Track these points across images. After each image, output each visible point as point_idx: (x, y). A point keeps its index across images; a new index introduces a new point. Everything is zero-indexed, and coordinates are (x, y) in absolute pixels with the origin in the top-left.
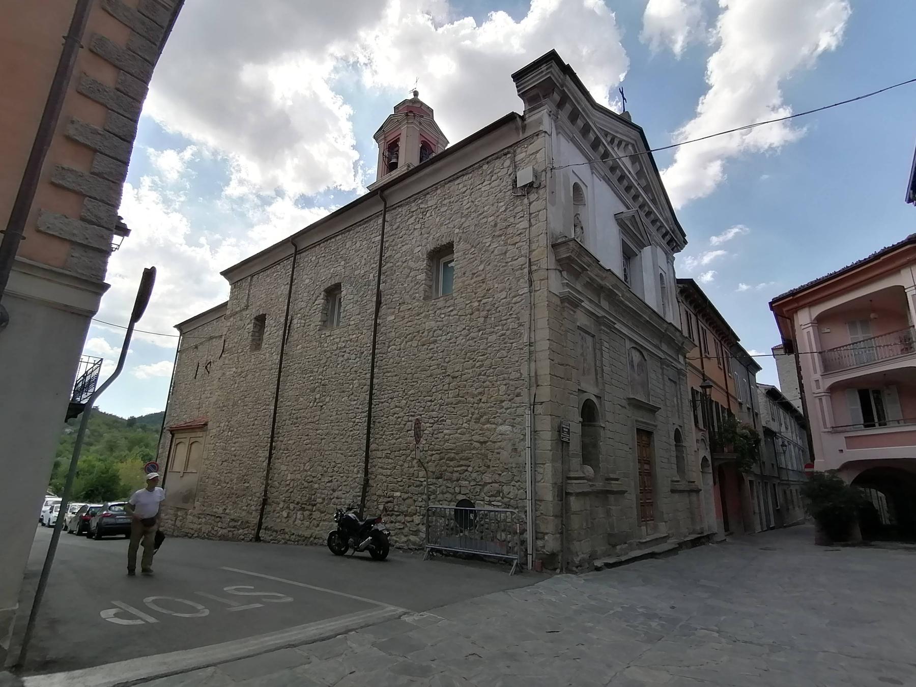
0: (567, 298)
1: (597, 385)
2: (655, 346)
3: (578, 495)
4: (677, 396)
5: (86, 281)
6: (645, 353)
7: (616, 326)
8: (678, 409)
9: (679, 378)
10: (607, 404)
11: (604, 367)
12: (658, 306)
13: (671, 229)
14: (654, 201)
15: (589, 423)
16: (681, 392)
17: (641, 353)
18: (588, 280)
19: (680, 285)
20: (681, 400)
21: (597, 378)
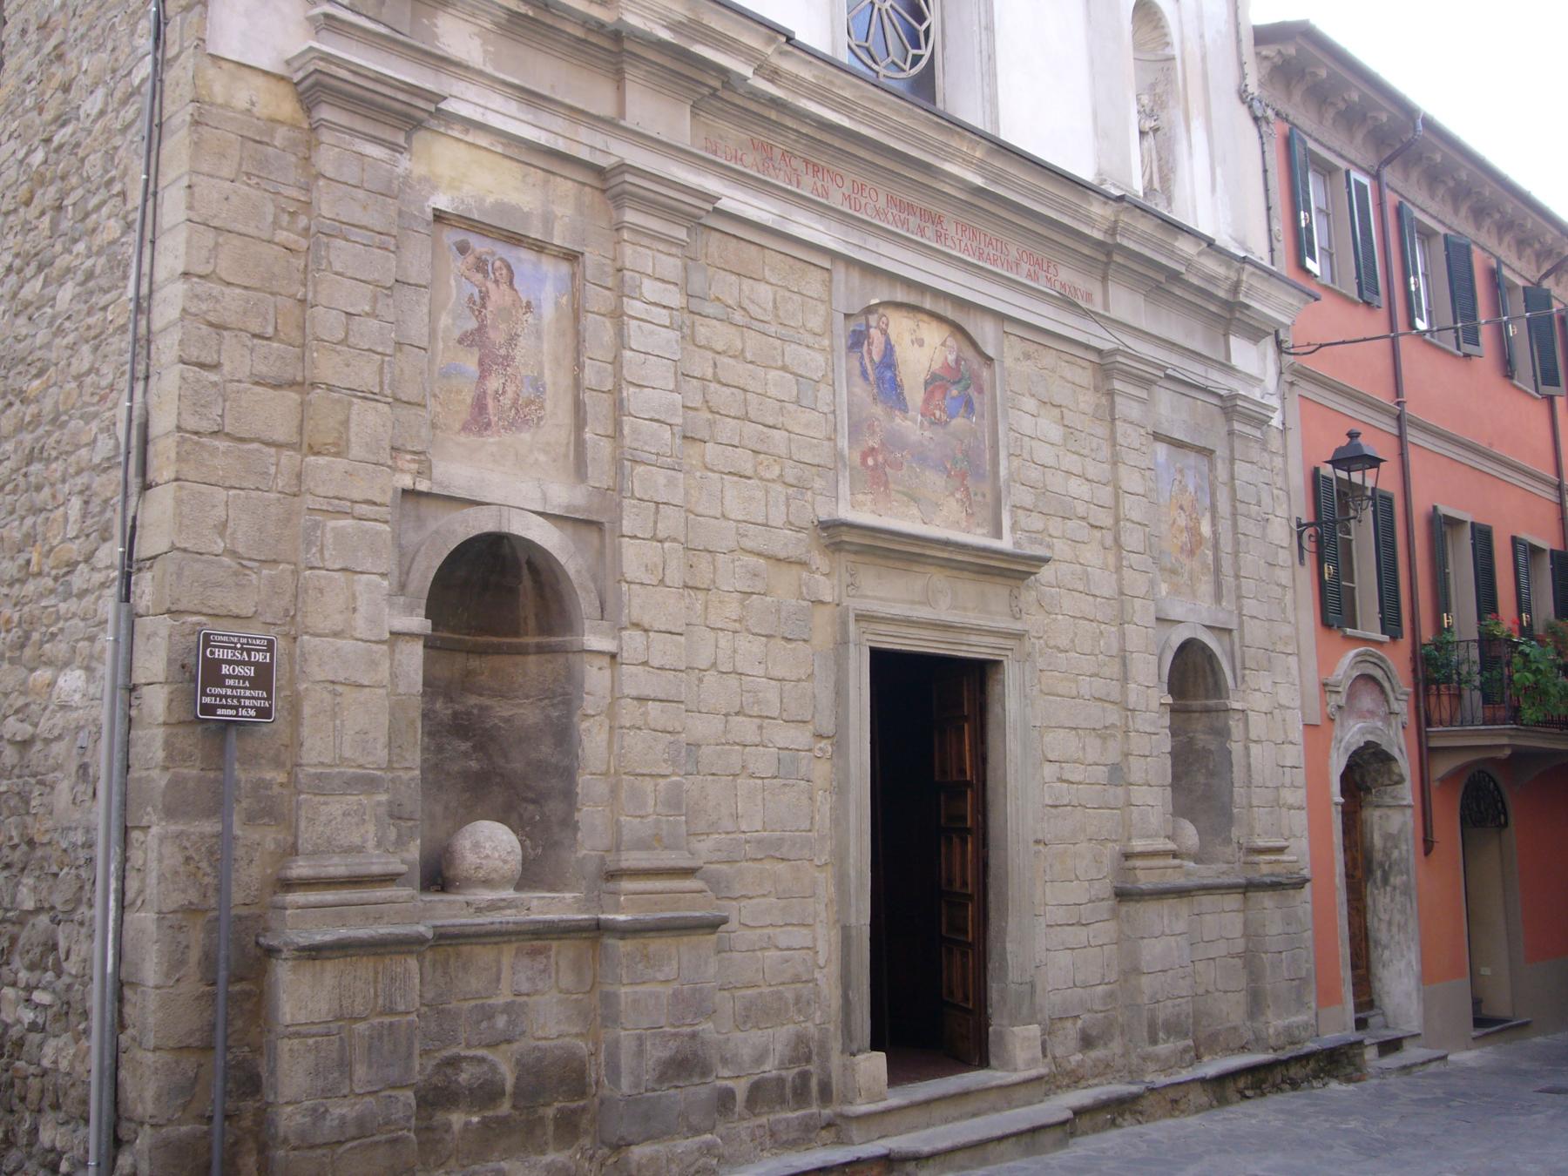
0: (317, 84)
1: (580, 467)
2: (1068, 303)
3: (315, 953)
4: (1213, 508)
5: (116, 1103)
6: (971, 324)
7: (724, 204)
8: (1217, 560)
9: (1231, 433)
10: (634, 558)
11: (629, 392)
12: (1101, 132)
15: (544, 640)
16: (1233, 490)
17: (958, 329)
19: (1265, 52)
20: (1235, 525)
21: (580, 444)
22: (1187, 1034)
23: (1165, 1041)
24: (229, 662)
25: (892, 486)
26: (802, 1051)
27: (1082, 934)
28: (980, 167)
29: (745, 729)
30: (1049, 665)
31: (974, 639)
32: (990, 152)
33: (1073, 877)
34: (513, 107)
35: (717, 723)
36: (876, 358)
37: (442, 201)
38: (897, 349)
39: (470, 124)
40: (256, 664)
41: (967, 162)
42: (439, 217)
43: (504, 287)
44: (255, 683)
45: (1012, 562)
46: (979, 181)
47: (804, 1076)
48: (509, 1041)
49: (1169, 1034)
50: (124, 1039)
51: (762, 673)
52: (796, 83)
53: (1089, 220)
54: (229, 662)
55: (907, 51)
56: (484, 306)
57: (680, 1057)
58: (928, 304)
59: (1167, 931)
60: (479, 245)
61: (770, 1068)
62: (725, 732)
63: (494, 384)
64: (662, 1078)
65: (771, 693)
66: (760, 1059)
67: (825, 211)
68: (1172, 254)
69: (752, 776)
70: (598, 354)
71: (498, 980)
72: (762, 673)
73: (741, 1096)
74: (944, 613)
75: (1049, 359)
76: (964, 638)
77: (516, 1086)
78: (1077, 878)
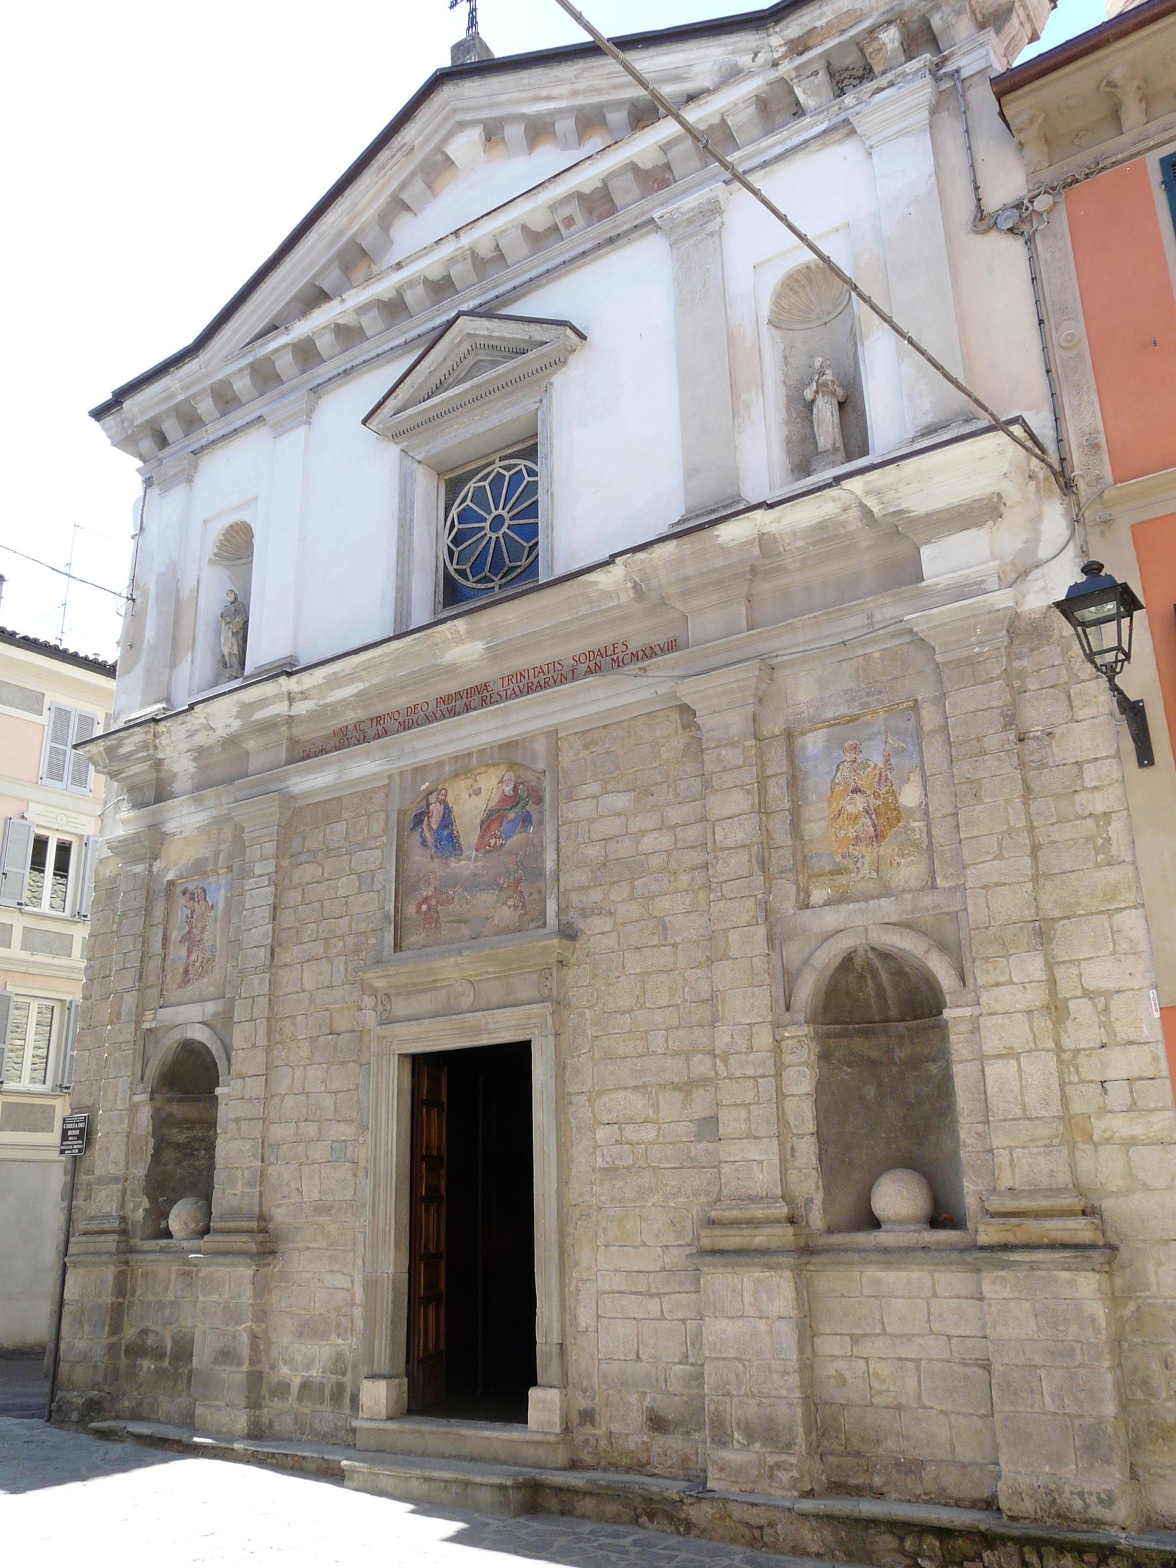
22: (789, 1446)
23: (745, 1448)
24: (71, 1129)
25: (442, 920)
26: (339, 1365)
35: (292, 1127)
36: (434, 826)
38: (455, 809)
40: (80, 1129)
43: (202, 902)
44: (80, 1137)
47: (340, 1386)
48: (171, 1324)
49: (751, 1438)
51: (322, 1089)
54: (71, 1129)
55: (530, 548)
56: (192, 918)
57: (225, 1350)
59: (749, 1311)
61: (315, 1373)
63: (194, 957)
64: (216, 1361)
65: (328, 1102)
66: (308, 1366)
70: (732, 756)
71: (168, 1288)
72: (322, 1089)
73: (295, 1389)
77: (172, 1348)
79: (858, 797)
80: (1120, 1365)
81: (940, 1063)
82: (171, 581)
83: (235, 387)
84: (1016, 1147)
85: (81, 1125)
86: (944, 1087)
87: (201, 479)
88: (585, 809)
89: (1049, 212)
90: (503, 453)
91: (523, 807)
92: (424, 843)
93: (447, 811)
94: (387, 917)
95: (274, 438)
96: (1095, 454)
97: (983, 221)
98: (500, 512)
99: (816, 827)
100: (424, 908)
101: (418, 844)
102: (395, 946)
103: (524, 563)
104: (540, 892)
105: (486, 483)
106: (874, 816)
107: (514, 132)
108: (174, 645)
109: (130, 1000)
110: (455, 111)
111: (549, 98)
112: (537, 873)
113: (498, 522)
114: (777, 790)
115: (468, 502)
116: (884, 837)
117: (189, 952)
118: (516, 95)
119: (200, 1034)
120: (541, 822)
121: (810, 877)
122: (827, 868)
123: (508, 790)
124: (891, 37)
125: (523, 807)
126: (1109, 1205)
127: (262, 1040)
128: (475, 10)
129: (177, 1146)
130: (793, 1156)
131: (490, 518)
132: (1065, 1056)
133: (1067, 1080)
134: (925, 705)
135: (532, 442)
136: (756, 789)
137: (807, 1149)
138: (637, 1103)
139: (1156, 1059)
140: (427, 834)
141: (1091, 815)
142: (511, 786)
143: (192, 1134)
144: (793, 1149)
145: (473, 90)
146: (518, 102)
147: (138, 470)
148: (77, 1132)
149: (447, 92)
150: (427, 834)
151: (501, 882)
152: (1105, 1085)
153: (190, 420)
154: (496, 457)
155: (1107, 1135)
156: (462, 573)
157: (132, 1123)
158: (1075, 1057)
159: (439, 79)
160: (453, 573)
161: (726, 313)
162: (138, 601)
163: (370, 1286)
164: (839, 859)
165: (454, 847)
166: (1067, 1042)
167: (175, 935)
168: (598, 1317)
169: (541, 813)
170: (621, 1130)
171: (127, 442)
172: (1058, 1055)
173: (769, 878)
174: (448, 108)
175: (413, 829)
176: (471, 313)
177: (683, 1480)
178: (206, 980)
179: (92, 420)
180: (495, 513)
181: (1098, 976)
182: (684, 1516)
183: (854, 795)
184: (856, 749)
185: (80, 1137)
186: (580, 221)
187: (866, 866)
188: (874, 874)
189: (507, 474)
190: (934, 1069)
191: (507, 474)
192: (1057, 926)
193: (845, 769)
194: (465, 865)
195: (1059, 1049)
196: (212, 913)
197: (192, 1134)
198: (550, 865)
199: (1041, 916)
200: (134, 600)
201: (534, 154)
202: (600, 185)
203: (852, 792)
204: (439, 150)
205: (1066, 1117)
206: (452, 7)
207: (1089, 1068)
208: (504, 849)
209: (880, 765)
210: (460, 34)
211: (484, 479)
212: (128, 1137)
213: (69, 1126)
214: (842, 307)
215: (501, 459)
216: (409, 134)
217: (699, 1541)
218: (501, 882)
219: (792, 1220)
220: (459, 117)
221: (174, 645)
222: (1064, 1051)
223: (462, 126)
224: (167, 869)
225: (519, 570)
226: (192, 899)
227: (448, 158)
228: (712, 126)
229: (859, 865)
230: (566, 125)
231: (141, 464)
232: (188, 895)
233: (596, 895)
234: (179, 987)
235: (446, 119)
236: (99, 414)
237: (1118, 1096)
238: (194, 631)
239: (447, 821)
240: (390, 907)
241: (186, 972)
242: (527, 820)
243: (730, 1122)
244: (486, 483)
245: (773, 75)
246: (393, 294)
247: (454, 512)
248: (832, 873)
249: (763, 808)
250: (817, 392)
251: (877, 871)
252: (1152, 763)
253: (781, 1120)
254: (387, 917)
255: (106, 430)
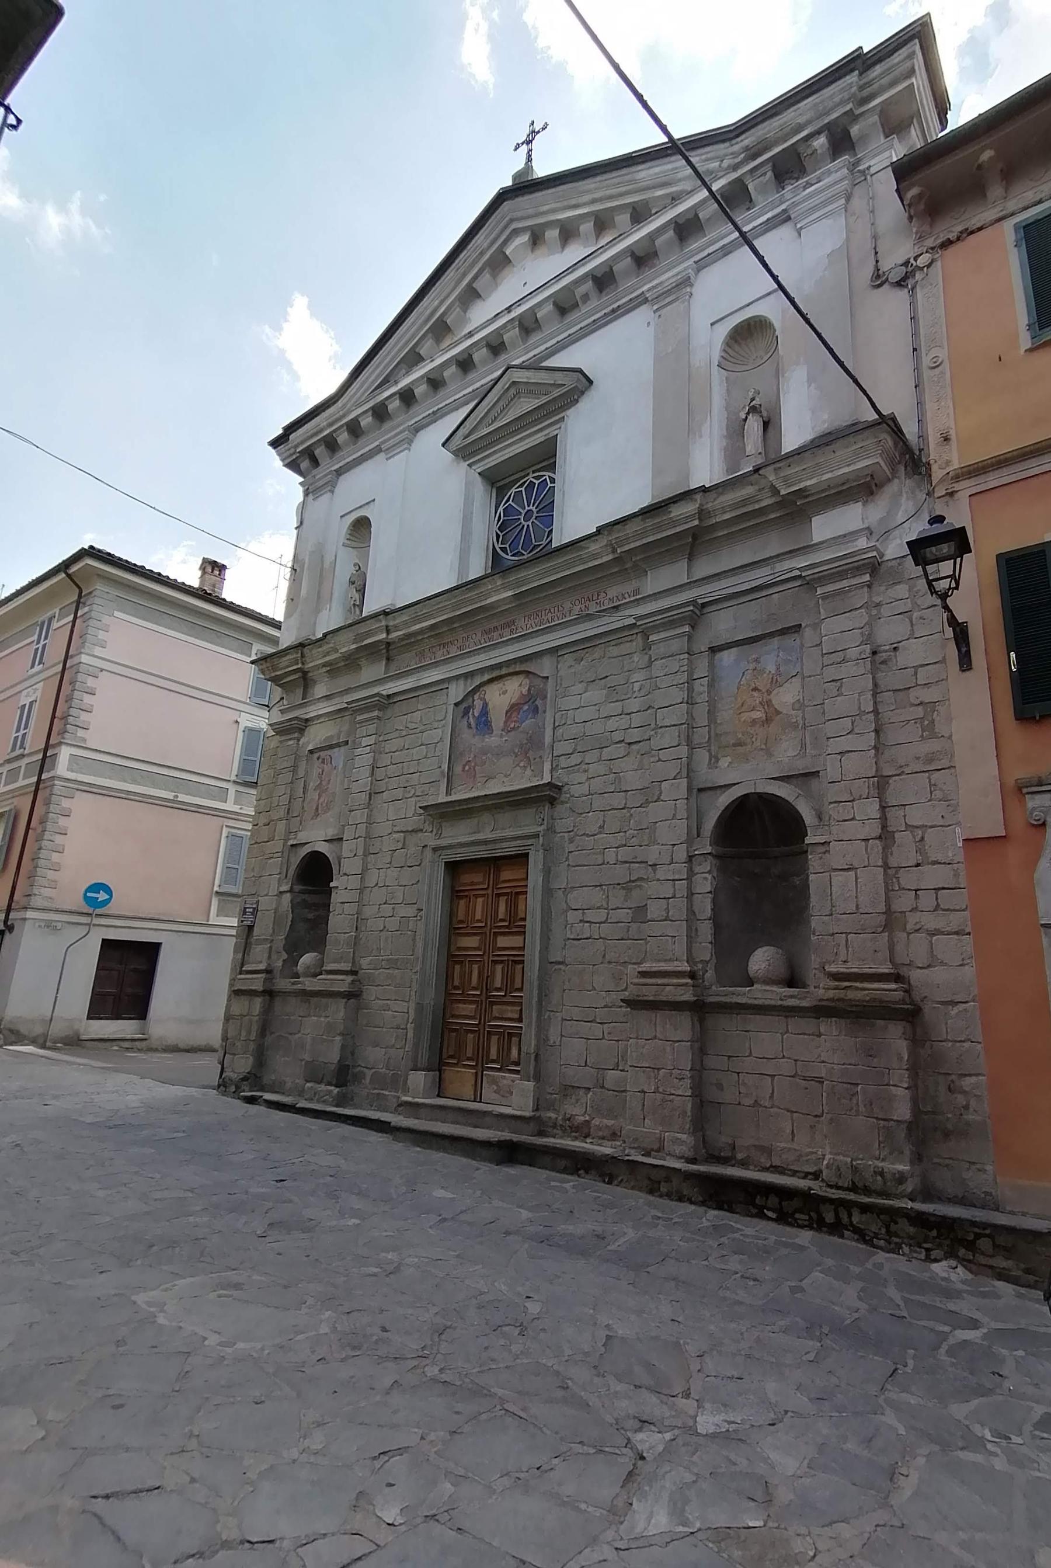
13: (735, 167)
14: (639, 214)
17: (528, 673)
18: (325, 669)
27: (597, 1030)
28: (505, 587)
29: (387, 910)
30: (821, 858)
31: (505, 845)
32: (503, 578)
33: (591, 988)
34: (325, 704)
36: (476, 714)
37: (310, 748)
39: (318, 717)
41: (497, 591)
42: (311, 752)
44: (252, 913)
45: (516, 796)
46: (510, 593)
50: (269, 1039)
52: (406, 624)
53: (595, 556)
58: (504, 671)
60: (323, 754)
62: (379, 912)
63: (322, 800)
67: (436, 664)
68: (674, 523)
69: (388, 931)
74: (486, 835)
75: (597, 653)
76: (498, 846)
78: (594, 989)
79: (756, 694)
80: (916, 1086)
81: (802, 876)
82: (319, 553)
83: (362, 424)
84: (850, 933)
85: (254, 906)
86: (804, 891)
87: (338, 490)
88: (571, 702)
89: (929, 266)
90: (534, 468)
91: (533, 702)
92: (469, 726)
93: (485, 705)
94: (443, 772)
95: (387, 459)
96: (947, 445)
97: (879, 279)
98: (531, 507)
99: (725, 714)
100: (467, 768)
101: (466, 726)
102: (447, 793)
103: (544, 543)
104: (541, 757)
105: (523, 489)
106: (766, 707)
107: (553, 234)
108: (319, 597)
109: (281, 826)
110: (512, 221)
111: (576, 206)
112: (540, 744)
113: (528, 514)
114: (701, 687)
115: (510, 502)
116: (772, 720)
117: (320, 796)
118: (553, 206)
119: (323, 848)
120: (545, 712)
121: (719, 748)
122: (732, 742)
123: (525, 691)
124: (821, 142)
125: (533, 702)
126: (916, 976)
127: (360, 852)
128: (531, 150)
129: (306, 920)
130: (696, 934)
131: (523, 512)
132: (890, 872)
133: (890, 888)
134: (807, 629)
135: (552, 461)
136: (686, 688)
137: (706, 930)
138: (597, 897)
139: (956, 875)
140: (471, 720)
141: (921, 704)
142: (527, 688)
143: (317, 913)
144: (696, 930)
145: (524, 202)
146: (554, 211)
147: (301, 484)
148: (251, 910)
149: (507, 206)
150: (471, 720)
151: (516, 751)
152: (918, 892)
153: (331, 445)
154: (531, 470)
155: (918, 927)
156: (504, 550)
157: (279, 904)
158: (897, 873)
159: (502, 197)
160: (499, 550)
161: (689, 358)
162: (298, 570)
163: (420, 1008)
164: (740, 736)
165: (488, 729)
166: (893, 862)
167: (312, 785)
168: (562, 1036)
169: (545, 705)
170: (583, 914)
171: (293, 465)
172: (885, 871)
173: (691, 747)
174: (507, 219)
175: (463, 717)
176: (520, 367)
177: (612, 1147)
178: (328, 814)
179: (270, 448)
180: (530, 523)
181: (916, 816)
182: (647, 1488)
183: (754, 693)
184: (757, 661)
185: (252, 913)
186: (593, 294)
187: (758, 741)
188: (763, 747)
189: (537, 482)
190: (797, 881)
191: (537, 482)
192: (891, 781)
193: (748, 676)
194: (493, 740)
195: (886, 866)
196: (335, 772)
197: (317, 913)
198: (548, 739)
199: (879, 774)
200: (295, 570)
201: (565, 252)
202: (608, 270)
203: (752, 690)
204: (501, 251)
205: (888, 912)
206: (515, 150)
207: (908, 880)
208: (521, 729)
209: (773, 672)
210: (520, 164)
211: (521, 486)
212: (275, 912)
213: (248, 906)
214: (770, 354)
215: (534, 472)
216: (480, 239)
217: (619, 1188)
218: (516, 751)
219: (692, 975)
220: (514, 226)
221: (319, 597)
222: (890, 868)
223: (516, 232)
224: (308, 743)
225: (541, 547)
226: (323, 762)
227: (507, 257)
228: (688, 220)
229: (754, 739)
230: (587, 227)
231: (301, 479)
232: (320, 760)
233: (575, 759)
234: (312, 819)
235: (506, 227)
236: (275, 443)
237: (927, 901)
238: (332, 588)
239: (485, 712)
240: (445, 767)
241: (317, 809)
242: (536, 710)
243: (655, 910)
244: (523, 489)
245: (734, 175)
246: (466, 356)
247: (501, 509)
248: (734, 745)
249: (690, 702)
250: (748, 413)
251: (766, 744)
252: (969, 668)
253: (691, 911)
254: (443, 772)
255: (279, 455)
